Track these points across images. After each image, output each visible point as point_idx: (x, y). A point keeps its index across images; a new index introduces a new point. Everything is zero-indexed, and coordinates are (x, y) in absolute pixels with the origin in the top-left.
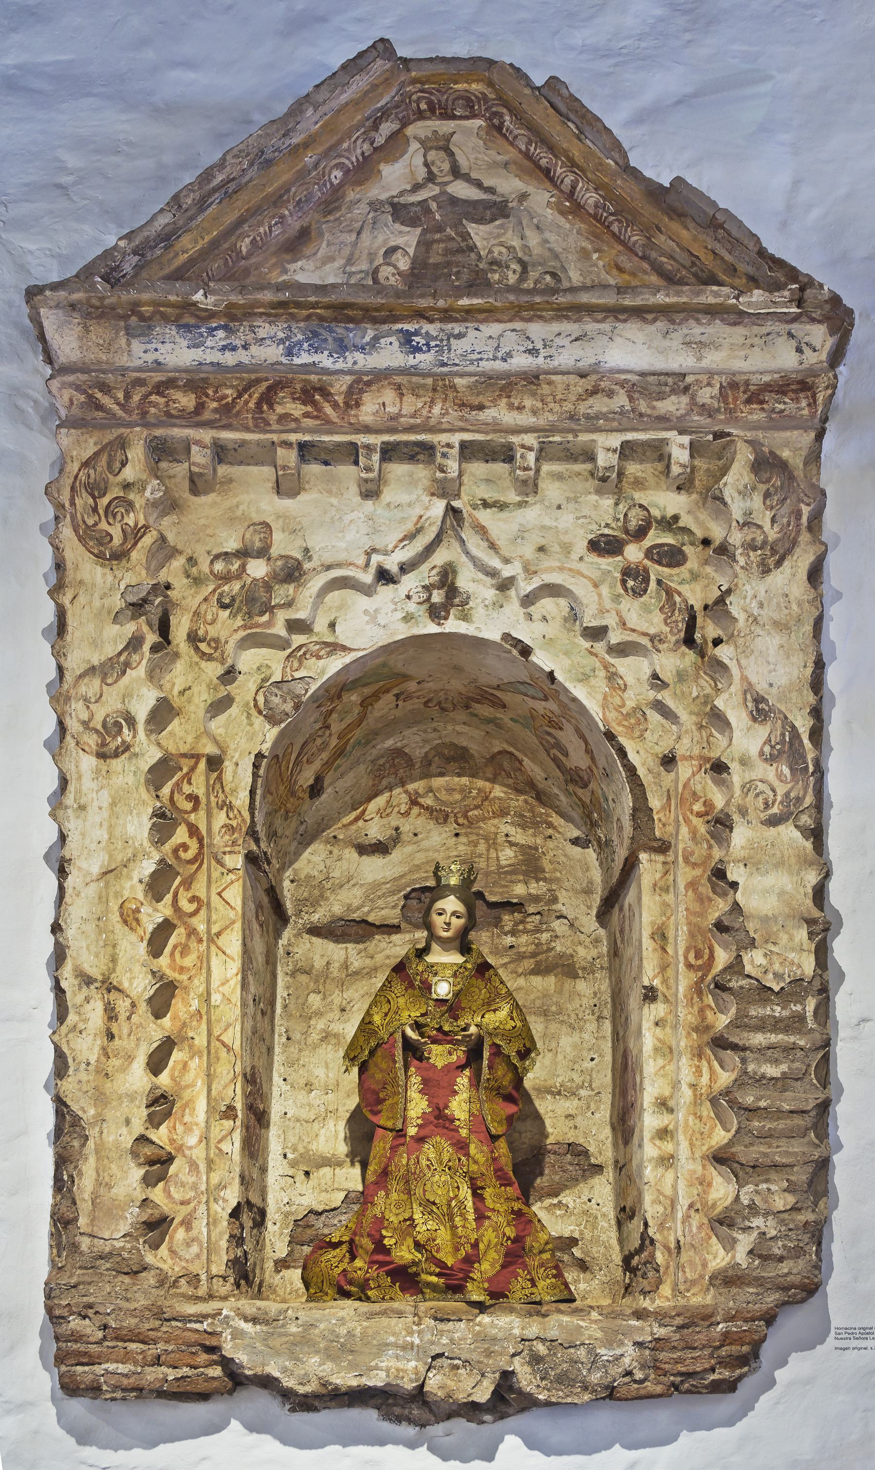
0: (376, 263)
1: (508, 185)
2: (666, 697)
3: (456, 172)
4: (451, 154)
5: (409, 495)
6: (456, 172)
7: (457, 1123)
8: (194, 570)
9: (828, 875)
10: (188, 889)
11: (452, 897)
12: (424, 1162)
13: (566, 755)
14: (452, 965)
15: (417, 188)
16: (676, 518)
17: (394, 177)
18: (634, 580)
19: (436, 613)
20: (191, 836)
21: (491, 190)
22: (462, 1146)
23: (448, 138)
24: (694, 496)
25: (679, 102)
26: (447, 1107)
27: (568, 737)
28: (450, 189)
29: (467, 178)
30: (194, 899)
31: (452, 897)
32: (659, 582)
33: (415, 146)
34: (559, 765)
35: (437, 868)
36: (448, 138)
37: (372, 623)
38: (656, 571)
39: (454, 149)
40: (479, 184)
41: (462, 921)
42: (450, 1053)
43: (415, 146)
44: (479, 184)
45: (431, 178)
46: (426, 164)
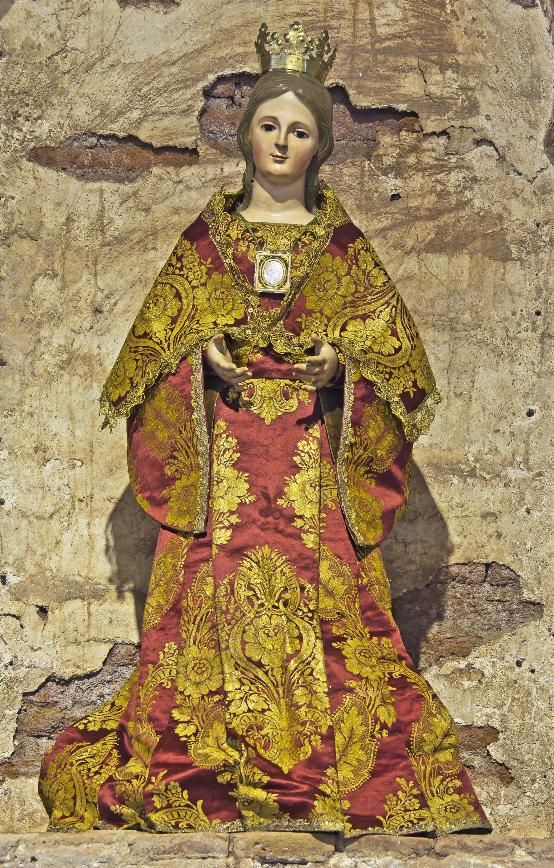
7: (299, 523)
11: (290, 96)
14: (290, 227)
22: (306, 565)
26: (281, 494)
31: (290, 96)
41: (308, 143)
42: (287, 396)
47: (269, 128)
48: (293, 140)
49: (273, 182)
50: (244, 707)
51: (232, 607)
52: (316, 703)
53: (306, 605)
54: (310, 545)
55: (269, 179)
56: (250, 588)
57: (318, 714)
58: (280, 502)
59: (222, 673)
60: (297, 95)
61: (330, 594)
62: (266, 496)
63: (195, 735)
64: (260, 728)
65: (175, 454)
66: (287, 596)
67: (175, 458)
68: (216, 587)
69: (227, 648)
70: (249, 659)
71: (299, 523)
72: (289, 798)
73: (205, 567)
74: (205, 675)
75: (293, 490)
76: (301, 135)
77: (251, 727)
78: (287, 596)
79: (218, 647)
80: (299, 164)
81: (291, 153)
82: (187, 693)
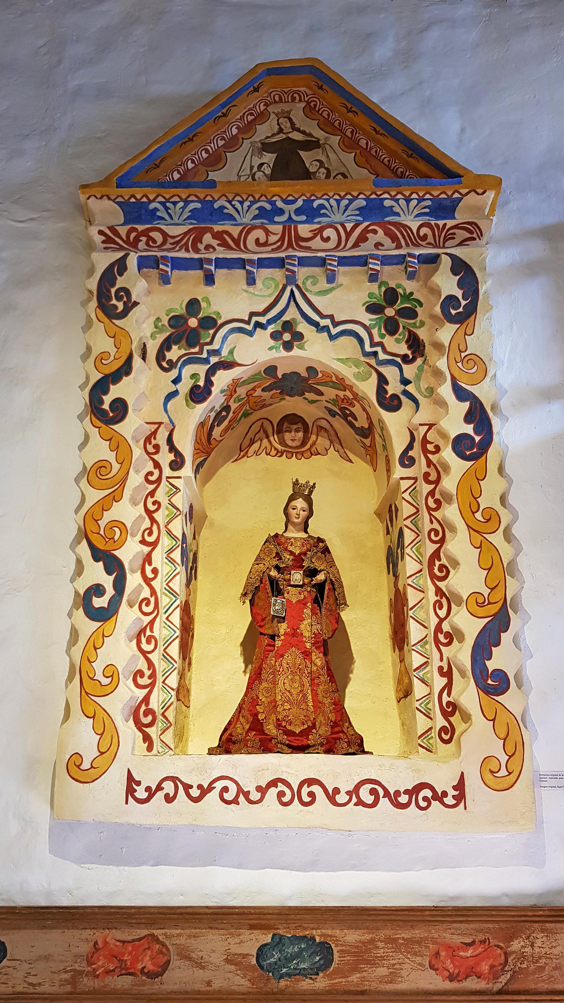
0: (254, 171)
1: (319, 134)
2: (410, 388)
3: (294, 128)
4: (290, 120)
5: (269, 280)
6: (294, 128)
7: (304, 639)
8: (160, 324)
9: (510, 486)
10: (152, 497)
11: (301, 499)
12: (285, 665)
13: (356, 420)
14: (301, 538)
15: (273, 135)
16: (411, 294)
17: (264, 131)
18: (391, 327)
19: (288, 346)
20: (155, 468)
21: (310, 135)
22: (307, 654)
23: (289, 112)
24: (420, 283)
25: (402, 94)
26: (298, 628)
27: (357, 409)
28: (290, 135)
29: (298, 130)
30: (154, 503)
31: (301, 499)
32: (404, 327)
33: (273, 116)
34: (352, 426)
35: (21, 884)
36: (289, 112)
37: (255, 352)
38: (402, 322)
39: (292, 117)
40: (304, 132)
41: (306, 513)
42: (300, 593)
43: (273, 116)
44: (304, 132)
45: (281, 131)
46: (278, 124)
47: (294, 509)
48: (302, 512)
49: (294, 524)
50: (282, 708)
51: (281, 670)
52: (309, 709)
53: (307, 670)
54: (308, 647)
55: (294, 524)
56: (288, 664)
57: (310, 713)
58: (298, 631)
59: (275, 693)
60: (303, 499)
61: (316, 665)
62: (293, 629)
63: (265, 718)
64: (288, 717)
65: (320, 676)
66: (300, 667)
67: (319, 678)
68: (276, 662)
69: (278, 684)
70: (286, 689)
71: (304, 639)
72: (452, 919)
73: (271, 654)
74: (269, 694)
75: (302, 627)
76: (304, 511)
77: (285, 717)
78: (300, 667)
79: (274, 684)
80: (303, 520)
81: (301, 517)
82: (263, 700)
